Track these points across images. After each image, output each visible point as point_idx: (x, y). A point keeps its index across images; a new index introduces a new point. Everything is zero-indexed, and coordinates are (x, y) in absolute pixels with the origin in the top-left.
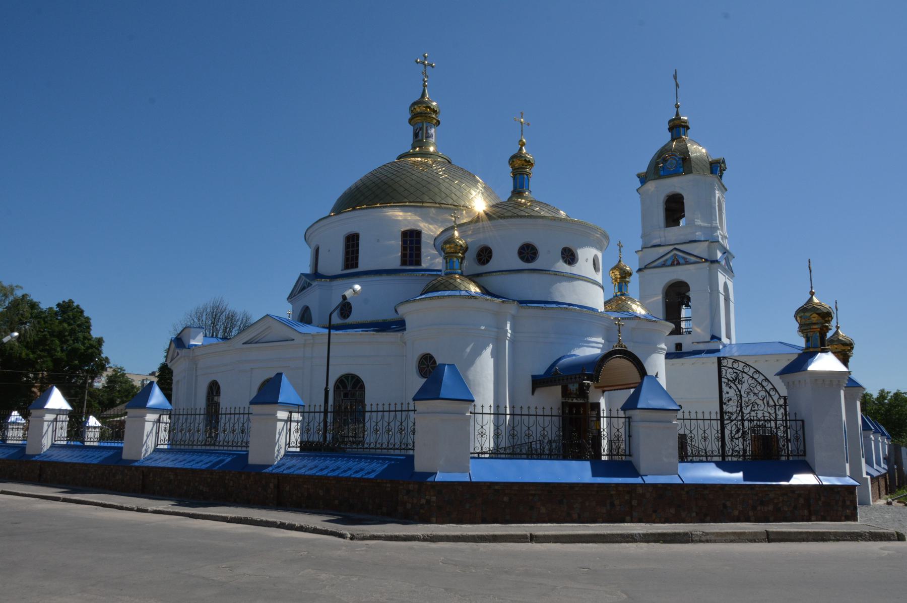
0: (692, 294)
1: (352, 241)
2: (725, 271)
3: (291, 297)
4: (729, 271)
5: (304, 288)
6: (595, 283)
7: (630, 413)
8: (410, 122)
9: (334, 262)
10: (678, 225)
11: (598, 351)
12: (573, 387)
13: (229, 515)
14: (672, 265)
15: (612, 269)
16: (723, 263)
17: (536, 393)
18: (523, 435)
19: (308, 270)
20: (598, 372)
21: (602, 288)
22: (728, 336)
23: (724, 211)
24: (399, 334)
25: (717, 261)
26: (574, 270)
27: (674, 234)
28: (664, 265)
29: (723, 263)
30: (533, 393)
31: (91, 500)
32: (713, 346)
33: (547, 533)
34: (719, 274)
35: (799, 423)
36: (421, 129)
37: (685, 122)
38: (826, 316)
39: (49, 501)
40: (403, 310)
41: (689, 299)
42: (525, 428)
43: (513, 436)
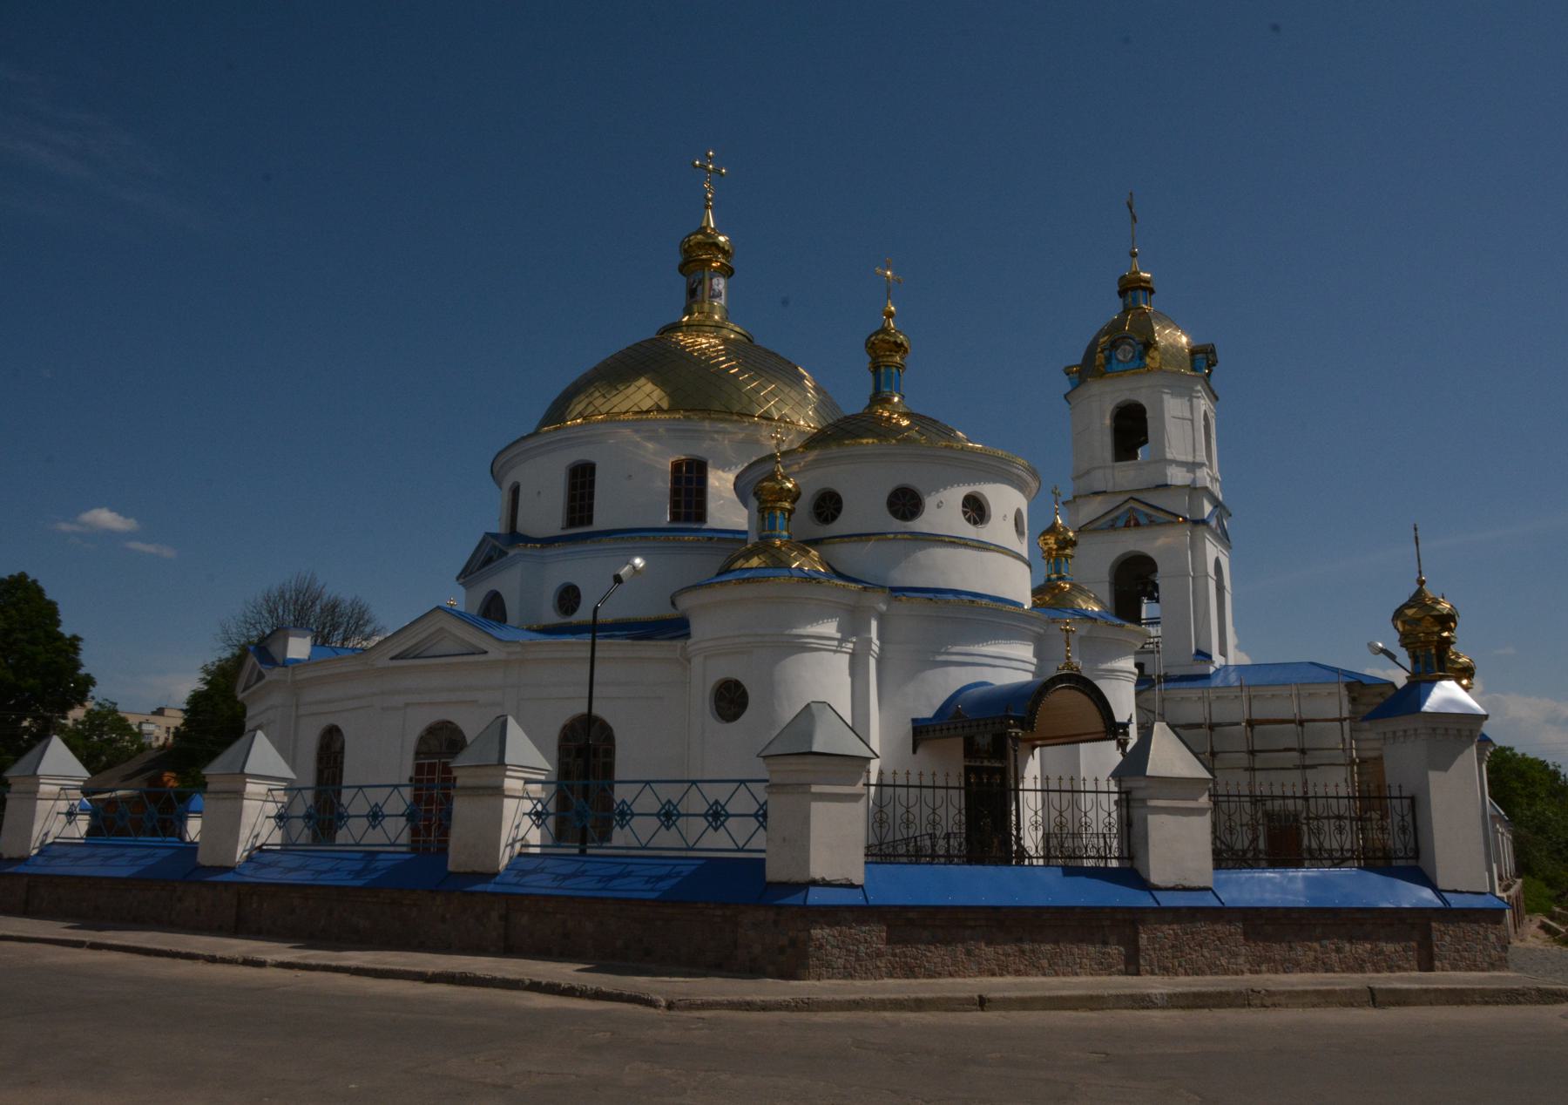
0: (1161, 579)
1: (582, 479)
2: (1215, 536)
3: (468, 575)
4: (1224, 538)
5: (489, 561)
6: (1018, 557)
7: (1129, 783)
8: (681, 270)
9: (545, 510)
10: (1135, 457)
11: (1028, 677)
12: (984, 741)
13: (430, 969)
14: (1127, 525)
15: (1044, 534)
16: (1213, 523)
17: (920, 751)
18: (898, 821)
19: (498, 527)
20: (1033, 713)
21: (1029, 566)
22: (1223, 653)
23: (1213, 436)
24: (679, 644)
25: (1204, 522)
26: (983, 533)
27: (1126, 476)
28: (1112, 527)
29: (1213, 523)
30: (914, 751)
31: (109, 942)
32: (1198, 669)
33: (1007, 994)
34: (1208, 544)
35: (1406, 802)
36: (701, 282)
37: (1146, 281)
38: (1447, 620)
39: (67, 949)
40: (686, 603)
41: (1156, 587)
42: (900, 810)
43: (881, 822)
